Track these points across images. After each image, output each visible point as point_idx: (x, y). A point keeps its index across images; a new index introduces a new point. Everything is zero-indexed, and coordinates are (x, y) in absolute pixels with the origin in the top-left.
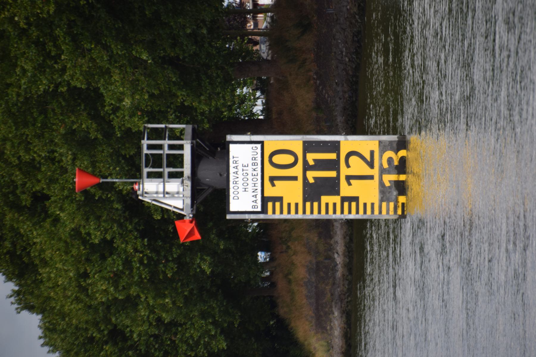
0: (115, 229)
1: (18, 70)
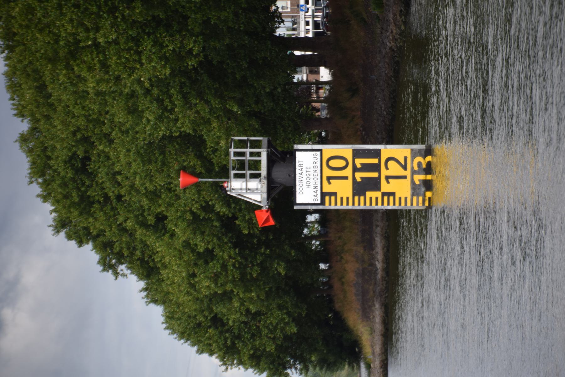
0: (215, 241)
1: (144, 120)
